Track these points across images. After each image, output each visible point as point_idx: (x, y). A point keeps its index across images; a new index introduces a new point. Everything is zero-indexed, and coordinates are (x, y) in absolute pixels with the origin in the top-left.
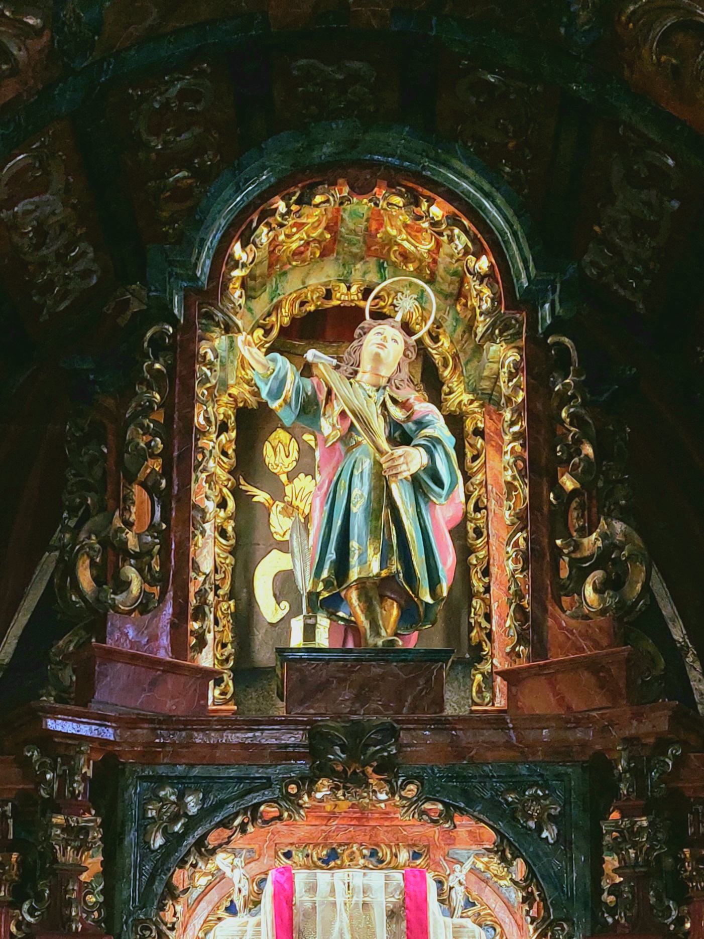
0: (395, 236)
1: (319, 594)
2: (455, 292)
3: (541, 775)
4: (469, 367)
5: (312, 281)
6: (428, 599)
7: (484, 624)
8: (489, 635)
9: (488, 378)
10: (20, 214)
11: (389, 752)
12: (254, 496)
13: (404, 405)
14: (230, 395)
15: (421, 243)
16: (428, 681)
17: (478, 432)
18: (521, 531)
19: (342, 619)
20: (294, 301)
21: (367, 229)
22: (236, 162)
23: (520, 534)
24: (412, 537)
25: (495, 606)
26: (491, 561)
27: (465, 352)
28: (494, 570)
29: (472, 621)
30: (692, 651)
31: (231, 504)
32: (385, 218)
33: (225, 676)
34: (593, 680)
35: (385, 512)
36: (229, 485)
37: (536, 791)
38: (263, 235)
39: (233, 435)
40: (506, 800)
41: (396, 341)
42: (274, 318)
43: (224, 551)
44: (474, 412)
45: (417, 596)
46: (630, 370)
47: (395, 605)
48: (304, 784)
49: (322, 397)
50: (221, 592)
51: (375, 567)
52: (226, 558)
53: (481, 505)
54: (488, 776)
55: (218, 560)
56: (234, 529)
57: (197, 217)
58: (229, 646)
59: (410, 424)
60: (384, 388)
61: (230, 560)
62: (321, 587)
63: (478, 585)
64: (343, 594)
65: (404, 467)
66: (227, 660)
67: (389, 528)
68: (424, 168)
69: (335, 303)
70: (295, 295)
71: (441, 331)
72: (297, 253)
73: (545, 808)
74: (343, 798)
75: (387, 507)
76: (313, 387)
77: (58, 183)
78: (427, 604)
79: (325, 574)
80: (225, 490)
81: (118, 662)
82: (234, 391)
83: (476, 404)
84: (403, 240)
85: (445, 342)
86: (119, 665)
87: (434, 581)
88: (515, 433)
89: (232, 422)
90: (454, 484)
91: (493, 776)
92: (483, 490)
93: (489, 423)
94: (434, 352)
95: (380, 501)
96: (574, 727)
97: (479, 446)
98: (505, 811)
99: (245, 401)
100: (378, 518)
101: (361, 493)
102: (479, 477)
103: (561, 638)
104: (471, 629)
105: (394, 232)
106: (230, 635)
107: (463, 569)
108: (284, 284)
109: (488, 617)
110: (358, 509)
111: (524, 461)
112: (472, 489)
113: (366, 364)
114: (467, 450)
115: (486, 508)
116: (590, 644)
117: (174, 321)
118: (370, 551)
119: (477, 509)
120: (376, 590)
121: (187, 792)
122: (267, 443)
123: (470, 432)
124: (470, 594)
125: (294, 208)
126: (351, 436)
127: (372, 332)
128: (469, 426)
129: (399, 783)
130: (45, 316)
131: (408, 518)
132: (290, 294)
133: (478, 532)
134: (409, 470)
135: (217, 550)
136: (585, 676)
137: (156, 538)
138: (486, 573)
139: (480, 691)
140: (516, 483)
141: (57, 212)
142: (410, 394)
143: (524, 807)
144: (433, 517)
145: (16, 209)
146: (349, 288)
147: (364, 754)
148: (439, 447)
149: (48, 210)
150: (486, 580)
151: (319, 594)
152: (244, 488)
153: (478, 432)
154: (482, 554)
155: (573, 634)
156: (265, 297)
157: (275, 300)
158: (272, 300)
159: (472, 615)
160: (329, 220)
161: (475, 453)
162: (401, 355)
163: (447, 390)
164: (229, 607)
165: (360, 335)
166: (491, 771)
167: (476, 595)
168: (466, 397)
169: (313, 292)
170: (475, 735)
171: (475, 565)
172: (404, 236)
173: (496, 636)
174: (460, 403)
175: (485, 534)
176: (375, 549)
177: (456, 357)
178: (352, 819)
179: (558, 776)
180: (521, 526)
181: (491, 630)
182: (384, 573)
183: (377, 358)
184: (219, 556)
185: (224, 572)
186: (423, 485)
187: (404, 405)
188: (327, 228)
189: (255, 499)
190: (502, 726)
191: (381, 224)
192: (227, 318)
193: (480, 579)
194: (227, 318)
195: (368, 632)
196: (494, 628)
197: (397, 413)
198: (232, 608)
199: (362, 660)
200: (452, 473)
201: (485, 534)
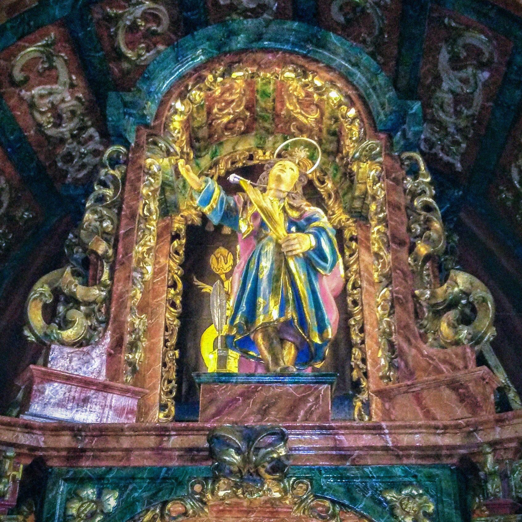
0: (292, 111)
1: (234, 337)
2: (335, 149)
3: (415, 476)
4: (345, 198)
5: (240, 148)
6: (317, 340)
7: (362, 366)
8: (366, 374)
9: (359, 197)
10: (36, 96)
11: (278, 454)
12: (202, 289)
13: (298, 209)
14: (182, 216)
15: (310, 114)
16: (317, 398)
17: (352, 239)
18: (387, 286)
19: (253, 357)
20: (228, 160)
21: (274, 109)
22: (176, 43)
23: (385, 289)
24: (303, 293)
25: (369, 353)
26: (365, 322)
27: (342, 189)
28: (368, 327)
29: (353, 364)
30: (513, 388)
31: (180, 286)
32: (285, 97)
33: (169, 404)
34: (454, 396)
35: (284, 278)
36: (179, 273)
37: (411, 491)
38: (197, 95)
39: (184, 241)
40: (386, 499)
41: (292, 169)
42: (213, 171)
43: (174, 316)
44: (350, 226)
45: (309, 337)
46: (458, 192)
47: (293, 346)
48: (207, 484)
49: (240, 206)
50: (169, 344)
51: (275, 313)
52: (173, 321)
53: (356, 285)
54: (369, 477)
55: (168, 322)
56: (181, 302)
57: (146, 75)
58: (174, 382)
59: (302, 221)
60: (284, 199)
61: (177, 322)
62: (234, 332)
63: (356, 338)
64: (252, 336)
65: (297, 246)
66: (171, 392)
67: (287, 289)
68: (309, 52)
69: (255, 162)
70: (228, 157)
71: (326, 177)
72: (227, 128)
73: (420, 507)
74: (242, 496)
75: (285, 274)
76: (235, 201)
77: (63, 75)
78: (316, 344)
79: (237, 321)
80: (175, 276)
81: (56, 382)
82: (185, 213)
83: (351, 221)
84: (298, 113)
85: (329, 185)
86: (56, 384)
87: (322, 329)
88: (379, 219)
89: (183, 233)
90: (335, 261)
91: (373, 477)
92: (358, 275)
93: (360, 232)
94: (322, 190)
95: (279, 269)
96: (442, 433)
97: (354, 247)
98: (385, 508)
99: (193, 220)
100: (278, 280)
101: (266, 264)
102: (355, 267)
103: (424, 364)
104: (352, 369)
105: (291, 108)
106: (174, 374)
107: (344, 328)
108: (222, 149)
109: (364, 361)
110: (264, 275)
111: (387, 237)
112: (349, 275)
113: (272, 185)
114: (345, 251)
115: (360, 287)
116: (448, 367)
117: (127, 144)
118: (272, 303)
119: (354, 287)
120: (278, 334)
121: (105, 492)
122: (213, 256)
123: (348, 240)
124: (350, 345)
125: (220, 79)
126: (261, 231)
127: (276, 165)
128: (347, 234)
129: (291, 482)
130: (69, 180)
131: (301, 282)
132: (225, 156)
133: (355, 303)
134: (301, 248)
135: (167, 315)
136: (447, 393)
137: (102, 291)
138: (362, 330)
139: (360, 415)
140: (382, 253)
141: (66, 100)
142: (304, 203)
143: (401, 504)
144: (321, 286)
145: (33, 92)
146: (264, 153)
147: (256, 455)
148: (323, 234)
149: (59, 97)
150: (362, 335)
151: (234, 337)
152: (196, 283)
153: (352, 239)
154: (358, 317)
155: (433, 359)
156: (208, 157)
157: (215, 159)
158: (213, 158)
159: (353, 360)
160: (248, 101)
161: (352, 252)
162: (297, 180)
163: (331, 213)
164: (174, 354)
165: (268, 168)
166: (371, 472)
167: (356, 345)
168: (344, 217)
169: (240, 155)
170: (355, 440)
171: (354, 326)
172: (299, 110)
173: (370, 374)
174: (340, 221)
175: (360, 304)
176: (275, 302)
177: (337, 192)
178: (265, 513)
179: (430, 477)
180: (387, 283)
181: (367, 369)
182: (282, 319)
183: (279, 179)
184: (169, 320)
185: (172, 330)
186: (313, 262)
187: (298, 209)
188: (247, 108)
189: (203, 291)
190: (379, 432)
191: (283, 104)
192: (168, 145)
193: (357, 335)
194: (168, 145)
195: (270, 362)
196: (369, 368)
197: (294, 214)
198: (177, 355)
199: (263, 382)
200: (334, 253)
201: (360, 304)
